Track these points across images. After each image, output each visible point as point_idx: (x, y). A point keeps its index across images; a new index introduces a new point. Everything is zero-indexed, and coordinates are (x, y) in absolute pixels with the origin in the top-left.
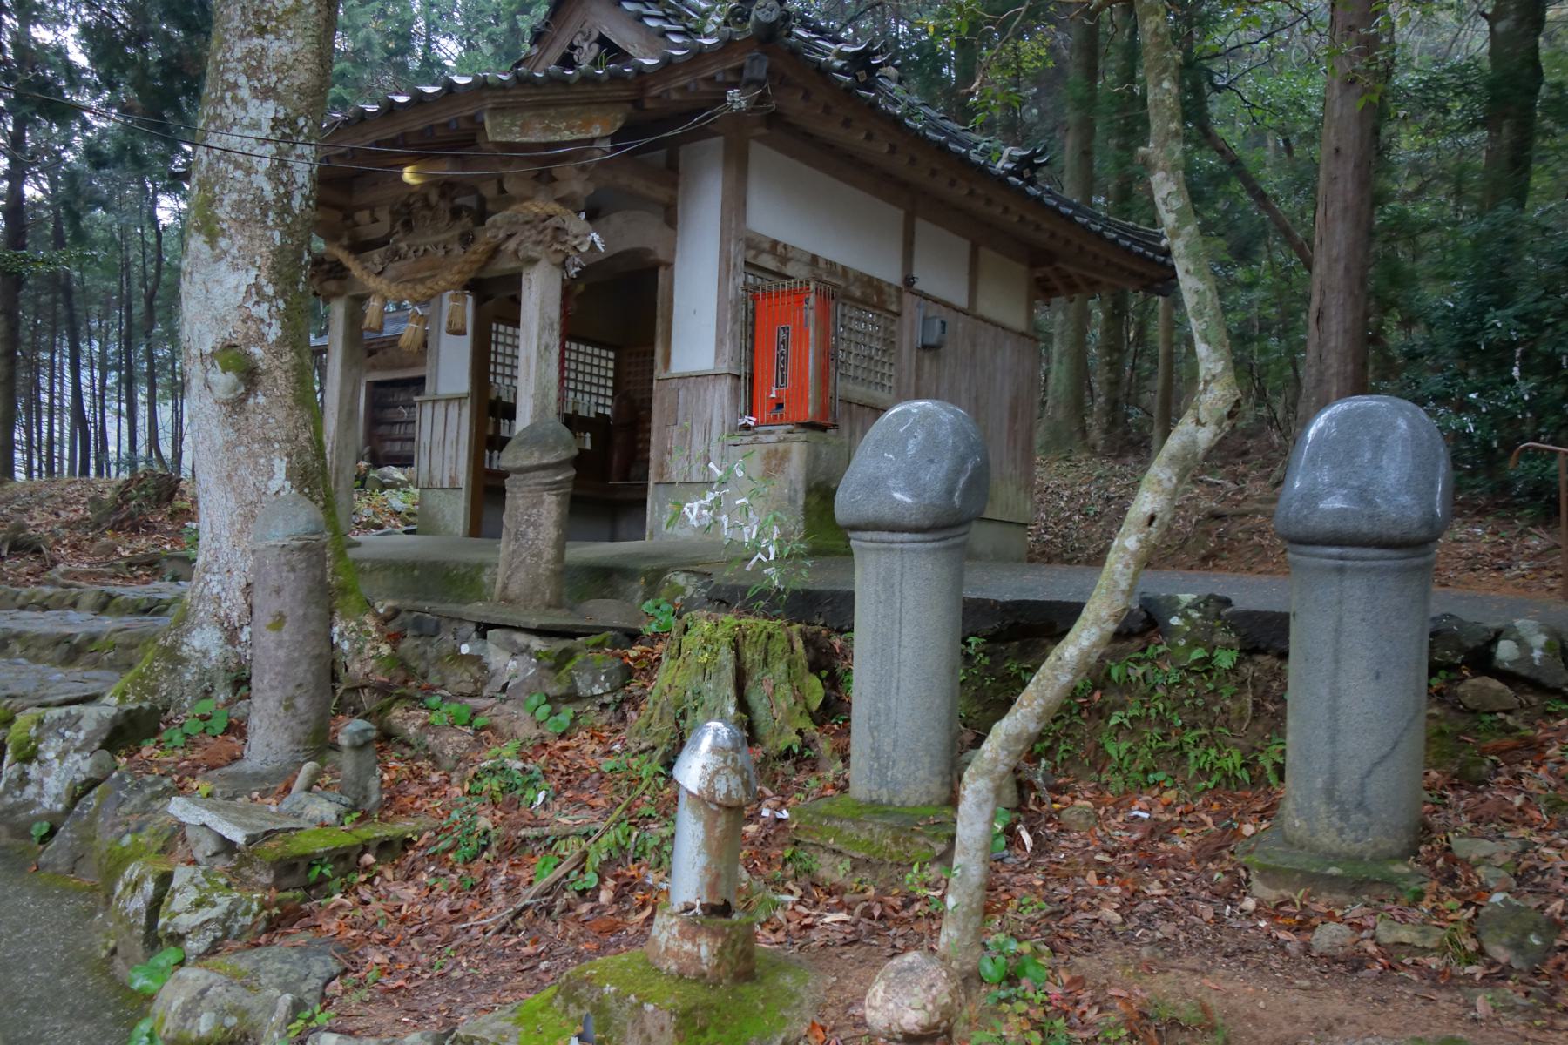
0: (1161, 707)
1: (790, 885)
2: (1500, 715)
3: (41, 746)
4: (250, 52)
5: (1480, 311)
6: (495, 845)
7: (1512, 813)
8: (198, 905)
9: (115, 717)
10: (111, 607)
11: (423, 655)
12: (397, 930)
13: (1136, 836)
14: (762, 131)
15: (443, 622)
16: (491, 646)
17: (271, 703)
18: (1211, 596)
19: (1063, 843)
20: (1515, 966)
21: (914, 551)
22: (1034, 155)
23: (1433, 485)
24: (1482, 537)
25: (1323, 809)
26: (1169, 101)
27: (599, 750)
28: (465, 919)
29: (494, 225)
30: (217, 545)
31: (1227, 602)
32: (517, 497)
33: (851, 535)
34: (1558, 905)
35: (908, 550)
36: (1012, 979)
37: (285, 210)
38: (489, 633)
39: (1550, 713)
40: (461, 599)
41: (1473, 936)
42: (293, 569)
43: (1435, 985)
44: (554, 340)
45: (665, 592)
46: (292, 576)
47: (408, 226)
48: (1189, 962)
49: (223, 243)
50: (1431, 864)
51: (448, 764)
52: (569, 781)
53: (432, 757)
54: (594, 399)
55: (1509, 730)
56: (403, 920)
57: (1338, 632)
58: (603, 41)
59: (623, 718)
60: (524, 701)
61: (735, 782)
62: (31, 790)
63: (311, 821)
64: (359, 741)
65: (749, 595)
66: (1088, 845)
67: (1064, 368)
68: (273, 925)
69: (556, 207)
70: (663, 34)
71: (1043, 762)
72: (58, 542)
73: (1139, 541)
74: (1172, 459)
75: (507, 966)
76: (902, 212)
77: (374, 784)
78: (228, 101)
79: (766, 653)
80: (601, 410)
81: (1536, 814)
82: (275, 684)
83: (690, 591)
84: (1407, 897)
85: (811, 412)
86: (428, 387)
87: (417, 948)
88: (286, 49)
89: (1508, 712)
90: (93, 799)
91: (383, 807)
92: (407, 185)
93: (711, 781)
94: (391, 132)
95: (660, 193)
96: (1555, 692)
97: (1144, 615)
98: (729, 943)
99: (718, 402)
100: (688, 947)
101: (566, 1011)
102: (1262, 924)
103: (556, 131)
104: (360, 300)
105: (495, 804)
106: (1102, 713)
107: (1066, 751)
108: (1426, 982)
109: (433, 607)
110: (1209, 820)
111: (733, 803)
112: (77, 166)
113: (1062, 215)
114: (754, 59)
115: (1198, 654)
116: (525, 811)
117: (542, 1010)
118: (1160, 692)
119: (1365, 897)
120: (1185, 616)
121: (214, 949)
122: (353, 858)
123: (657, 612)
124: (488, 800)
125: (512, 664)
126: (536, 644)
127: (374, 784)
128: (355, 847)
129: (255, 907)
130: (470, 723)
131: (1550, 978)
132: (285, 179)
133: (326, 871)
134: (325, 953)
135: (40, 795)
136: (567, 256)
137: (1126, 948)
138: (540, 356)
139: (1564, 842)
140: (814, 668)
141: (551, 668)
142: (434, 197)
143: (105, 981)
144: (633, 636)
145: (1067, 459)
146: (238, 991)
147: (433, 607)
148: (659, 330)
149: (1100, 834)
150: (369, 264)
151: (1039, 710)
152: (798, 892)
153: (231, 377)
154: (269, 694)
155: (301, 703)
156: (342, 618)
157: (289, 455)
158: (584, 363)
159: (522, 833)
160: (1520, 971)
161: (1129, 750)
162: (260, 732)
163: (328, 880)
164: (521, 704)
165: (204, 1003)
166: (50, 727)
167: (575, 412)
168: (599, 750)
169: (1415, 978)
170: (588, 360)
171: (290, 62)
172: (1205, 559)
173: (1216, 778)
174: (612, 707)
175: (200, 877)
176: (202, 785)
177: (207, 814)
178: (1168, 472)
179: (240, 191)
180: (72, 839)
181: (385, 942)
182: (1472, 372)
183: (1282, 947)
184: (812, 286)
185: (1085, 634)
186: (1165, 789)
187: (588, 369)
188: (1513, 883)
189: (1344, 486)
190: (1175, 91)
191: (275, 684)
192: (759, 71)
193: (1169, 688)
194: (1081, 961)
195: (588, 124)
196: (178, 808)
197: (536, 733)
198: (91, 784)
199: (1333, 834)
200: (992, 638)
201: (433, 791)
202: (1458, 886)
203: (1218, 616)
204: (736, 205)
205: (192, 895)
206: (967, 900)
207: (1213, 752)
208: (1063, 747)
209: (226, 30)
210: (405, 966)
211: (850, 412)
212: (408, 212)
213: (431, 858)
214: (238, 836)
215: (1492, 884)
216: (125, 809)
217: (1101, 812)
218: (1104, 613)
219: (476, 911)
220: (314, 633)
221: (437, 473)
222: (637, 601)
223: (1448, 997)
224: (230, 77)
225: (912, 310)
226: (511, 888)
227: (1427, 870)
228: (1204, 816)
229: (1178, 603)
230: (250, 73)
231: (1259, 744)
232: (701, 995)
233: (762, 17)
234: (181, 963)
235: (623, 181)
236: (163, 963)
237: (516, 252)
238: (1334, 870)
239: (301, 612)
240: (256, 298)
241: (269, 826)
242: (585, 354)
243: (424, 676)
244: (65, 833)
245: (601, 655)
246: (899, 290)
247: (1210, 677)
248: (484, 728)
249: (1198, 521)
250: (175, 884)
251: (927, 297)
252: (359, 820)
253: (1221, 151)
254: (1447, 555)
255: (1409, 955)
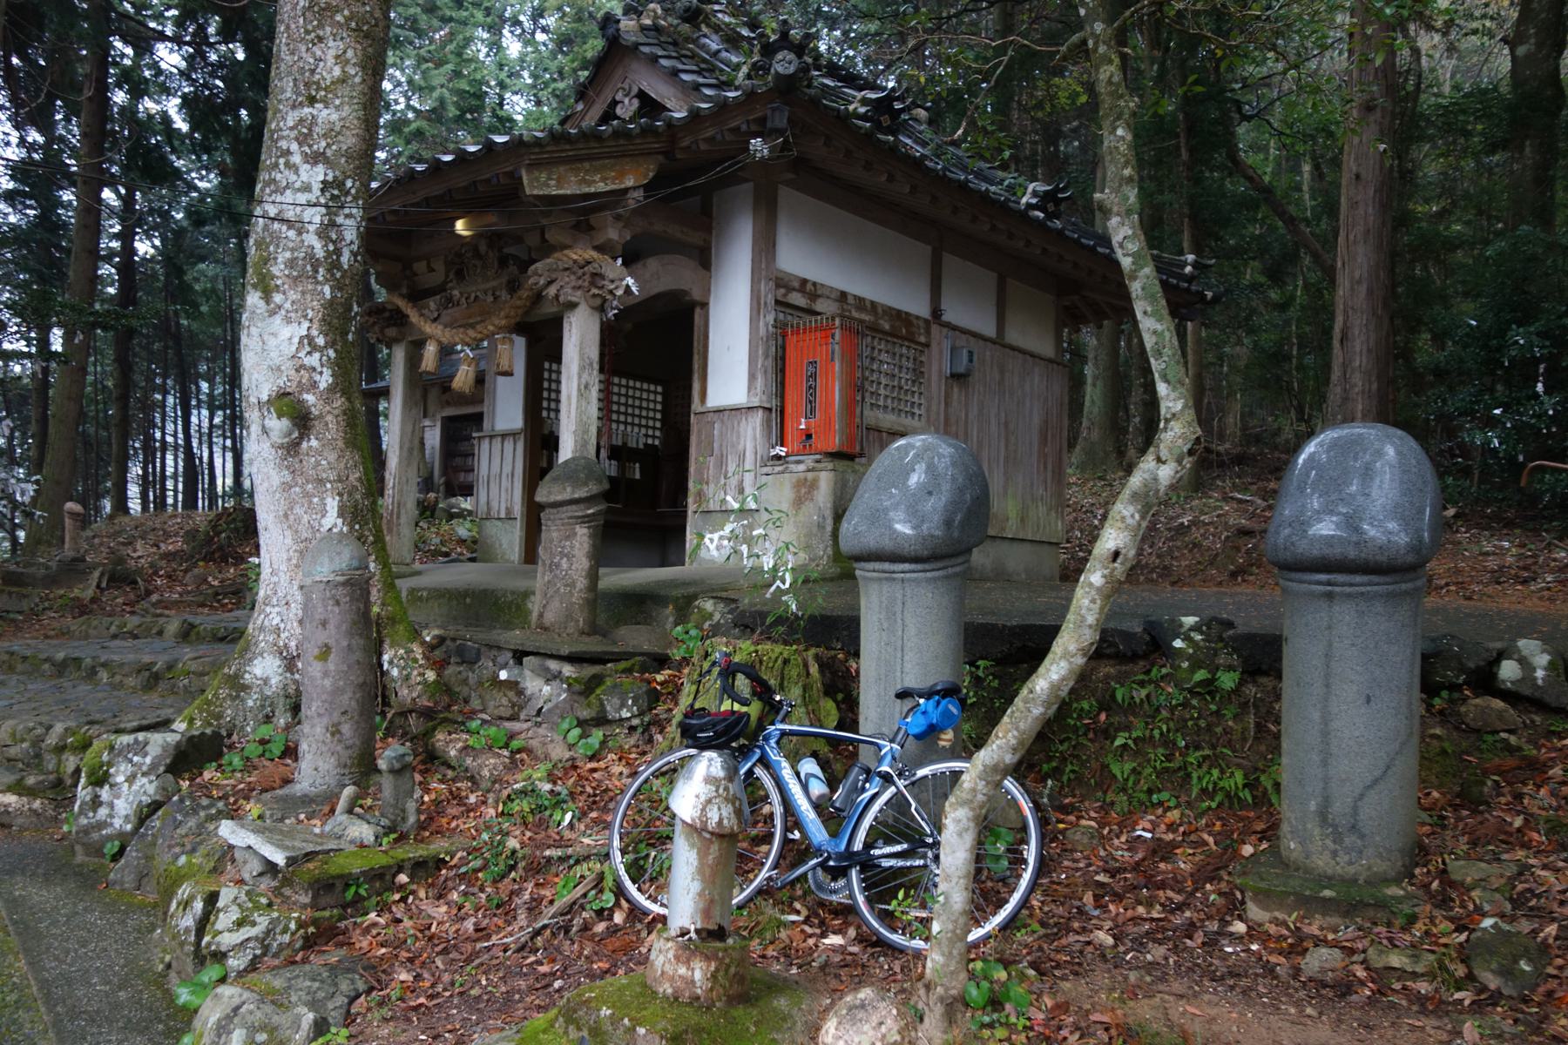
0: (1164, 728)
1: (797, 905)
2: (1503, 735)
3: (112, 771)
4: (301, 121)
5: (1502, 332)
6: (522, 865)
7: (1511, 834)
8: (240, 924)
9: (178, 744)
10: (193, 636)
11: (465, 682)
12: (423, 949)
13: (1140, 856)
14: (790, 176)
15: (483, 649)
16: (527, 673)
17: (318, 730)
18: (1214, 619)
19: (1066, 863)
20: (1506, 992)
21: (915, 580)
22: (1057, 190)
23: (1421, 511)
24: (1508, 550)
25: (1317, 831)
26: (1123, 148)
27: (626, 771)
28: (488, 937)
29: (536, 273)
30: (275, 579)
31: (1230, 625)
32: (552, 532)
33: (856, 565)
34: (1552, 929)
35: (909, 580)
36: (995, 1003)
37: (336, 265)
38: (525, 660)
39: (1553, 733)
40: (509, 626)
41: (1462, 961)
42: (338, 603)
43: (1424, 1012)
44: (594, 378)
45: (694, 617)
46: (337, 609)
47: (460, 275)
48: (1177, 986)
49: (278, 298)
50: (1426, 886)
51: (485, 785)
52: (594, 802)
53: (472, 779)
54: (643, 431)
55: (1510, 749)
56: (431, 938)
57: (1328, 656)
58: (642, 95)
59: (650, 741)
60: (557, 724)
61: (727, 811)
62: (103, 812)
63: (351, 842)
64: (397, 766)
65: (769, 621)
66: (1090, 865)
67: (1098, 391)
68: (309, 944)
69: (595, 254)
70: (697, 87)
71: (1050, 782)
72: (156, 573)
73: (1104, 576)
74: (1135, 496)
75: (523, 984)
76: (929, 248)
77: (411, 806)
78: (282, 167)
79: (782, 679)
80: (650, 441)
81: (1535, 836)
82: (322, 711)
83: (717, 617)
84: (1399, 922)
85: (836, 442)
86: (486, 425)
87: (441, 967)
88: (335, 117)
89: (1510, 732)
90: (156, 822)
91: (422, 826)
92: (460, 236)
93: (703, 810)
94: (437, 190)
95: (695, 238)
96: (1559, 711)
97: (1147, 638)
98: (723, 967)
99: (751, 435)
100: (682, 971)
101: (566, 1032)
102: (1254, 947)
103: (589, 183)
104: (418, 345)
105: (525, 824)
106: (1107, 734)
107: (1073, 771)
108: (1415, 1008)
109: (472, 636)
110: (1211, 840)
111: (727, 831)
112: (185, 224)
113: (1084, 247)
114: (774, 110)
115: (1201, 675)
116: (552, 832)
117: (545, 1031)
118: (1164, 713)
119: (1358, 920)
120: (1187, 639)
121: (253, 966)
122: (388, 877)
123: (685, 637)
124: (519, 821)
125: (547, 689)
126: (568, 670)
127: (411, 806)
128: (390, 867)
129: (293, 926)
130: (506, 746)
131: (1539, 1005)
132: (334, 237)
133: (363, 892)
134: (354, 971)
135: (111, 816)
136: (605, 300)
137: (1115, 972)
138: (580, 395)
139: (1561, 864)
140: (829, 691)
141: (580, 693)
142: (483, 248)
143: (159, 994)
144: (662, 661)
145: (1101, 478)
146: (268, 1008)
147: (472, 636)
148: (696, 366)
149: (1102, 853)
150: (426, 311)
151: (1013, 742)
152: (805, 912)
153: (285, 423)
154: (316, 720)
155: (346, 729)
156: (391, 646)
157: (340, 494)
158: (634, 397)
159: (547, 853)
160: (1511, 997)
161: (1134, 770)
162: (308, 757)
163: (364, 899)
164: (554, 727)
165: (236, 1020)
166: (121, 752)
167: (625, 444)
168: (626, 771)
169: (1404, 1003)
170: (638, 394)
171: (337, 128)
172: (1234, 575)
173: (1218, 798)
174: (640, 730)
175: (243, 897)
176: (253, 808)
177: (252, 836)
178: (1131, 509)
179: (293, 250)
180: (138, 858)
181: (411, 960)
182: (1499, 387)
183: (1272, 971)
184: (837, 322)
185: (1054, 668)
186: (1169, 809)
187: (637, 403)
188: (1508, 906)
189: (1331, 512)
190: (1129, 137)
191: (322, 711)
192: (780, 121)
193: (1172, 709)
194: (1066, 985)
195: (621, 176)
196: (228, 831)
197: (567, 755)
198: (155, 806)
199: (1327, 856)
200: (999, 662)
201: (469, 811)
202: (1452, 909)
203: (1221, 639)
204: (765, 248)
205: (234, 914)
206: (951, 927)
207: (1215, 772)
208: (1070, 767)
209: (280, 101)
210: (427, 984)
211: (881, 439)
212: (462, 259)
213: (462, 877)
214: (279, 858)
215: (1487, 907)
216: (182, 831)
217: (1105, 832)
218: (1072, 647)
219: (499, 929)
220: (358, 662)
221: (495, 505)
222: (668, 626)
223: (1436, 1023)
224: (283, 144)
225: (941, 344)
226: (534, 907)
227: (1420, 893)
228: (1206, 836)
229: (1181, 625)
230: (302, 140)
231: (1260, 765)
232: (694, 1018)
233: (780, 69)
234: (223, 980)
235: (658, 227)
236: (206, 979)
237: (557, 297)
238: (1327, 893)
239: (345, 643)
240: (308, 349)
241: (310, 848)
242: (634, 388)
243: (466, 701)
244: (132, 852)
245: (630, 680)
246: (926, 321)
247: (1213, 698)
248: (519, 751)
249: (1227, 538)
250: (220, 904)
251: (954, 328)
252: (396, 841)
253: (1250, 179)
254: (1473, 569)
255: (1398, 980)
